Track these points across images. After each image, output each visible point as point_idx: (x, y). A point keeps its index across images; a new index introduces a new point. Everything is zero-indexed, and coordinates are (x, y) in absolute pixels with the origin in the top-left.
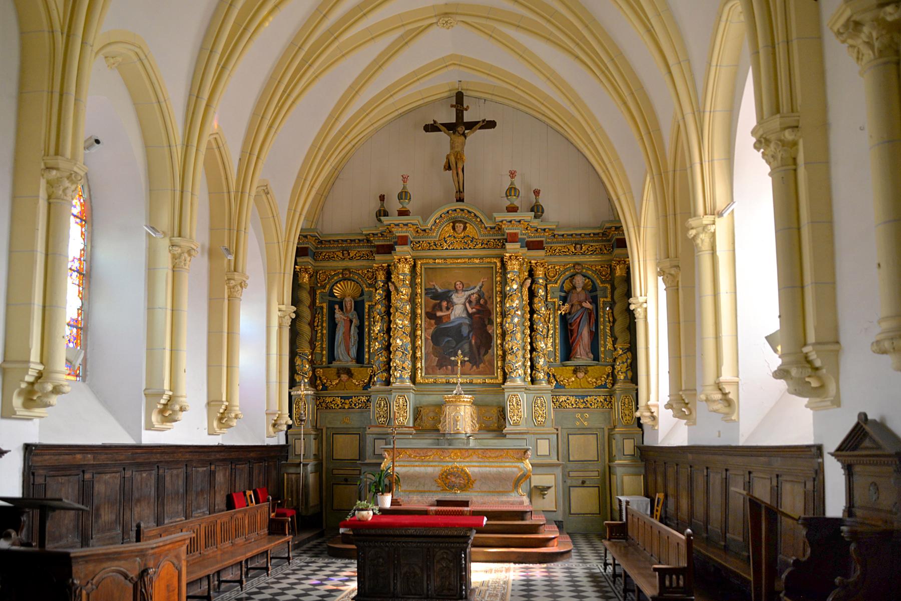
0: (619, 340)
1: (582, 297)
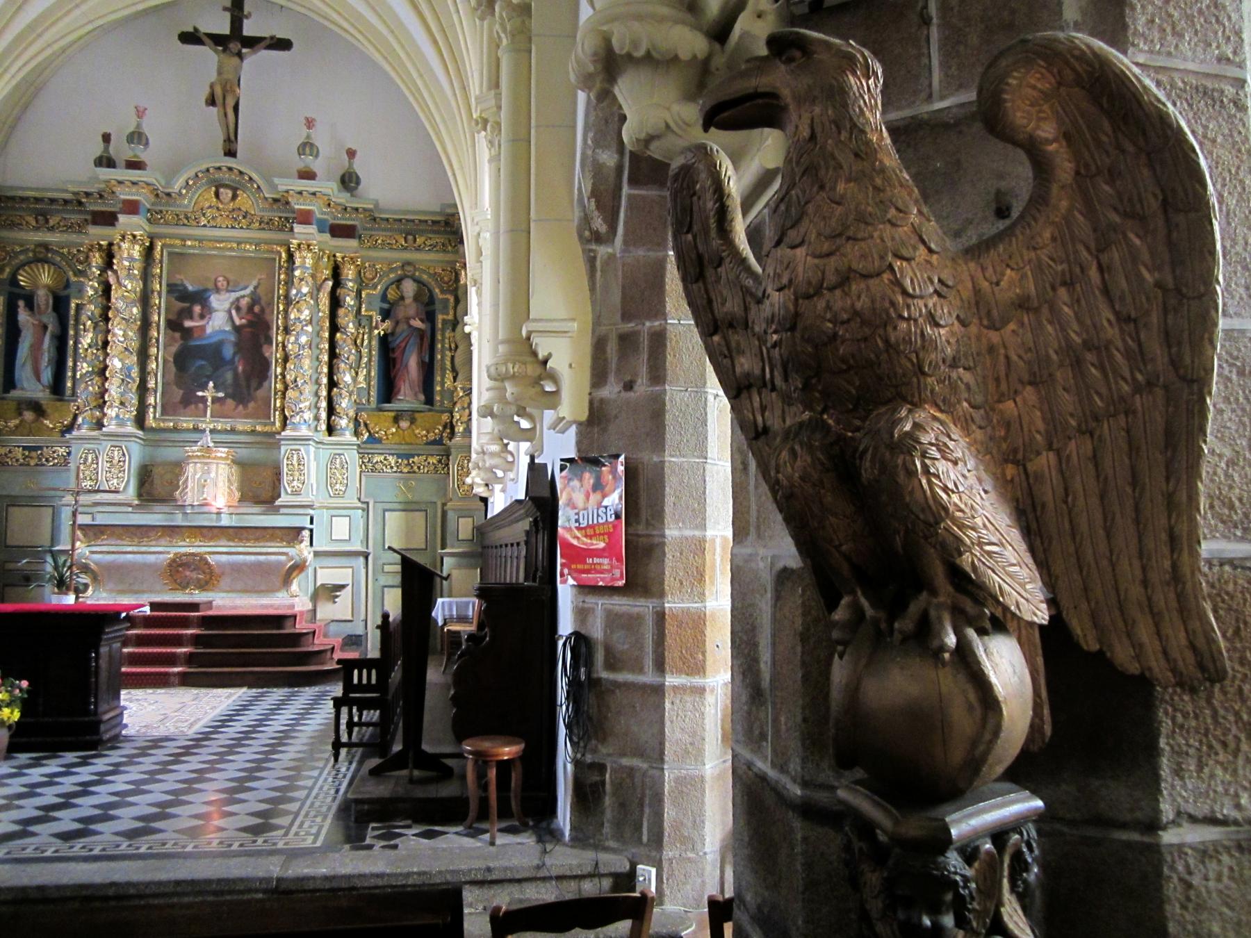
0: (460, 377)
1: (412, 311)
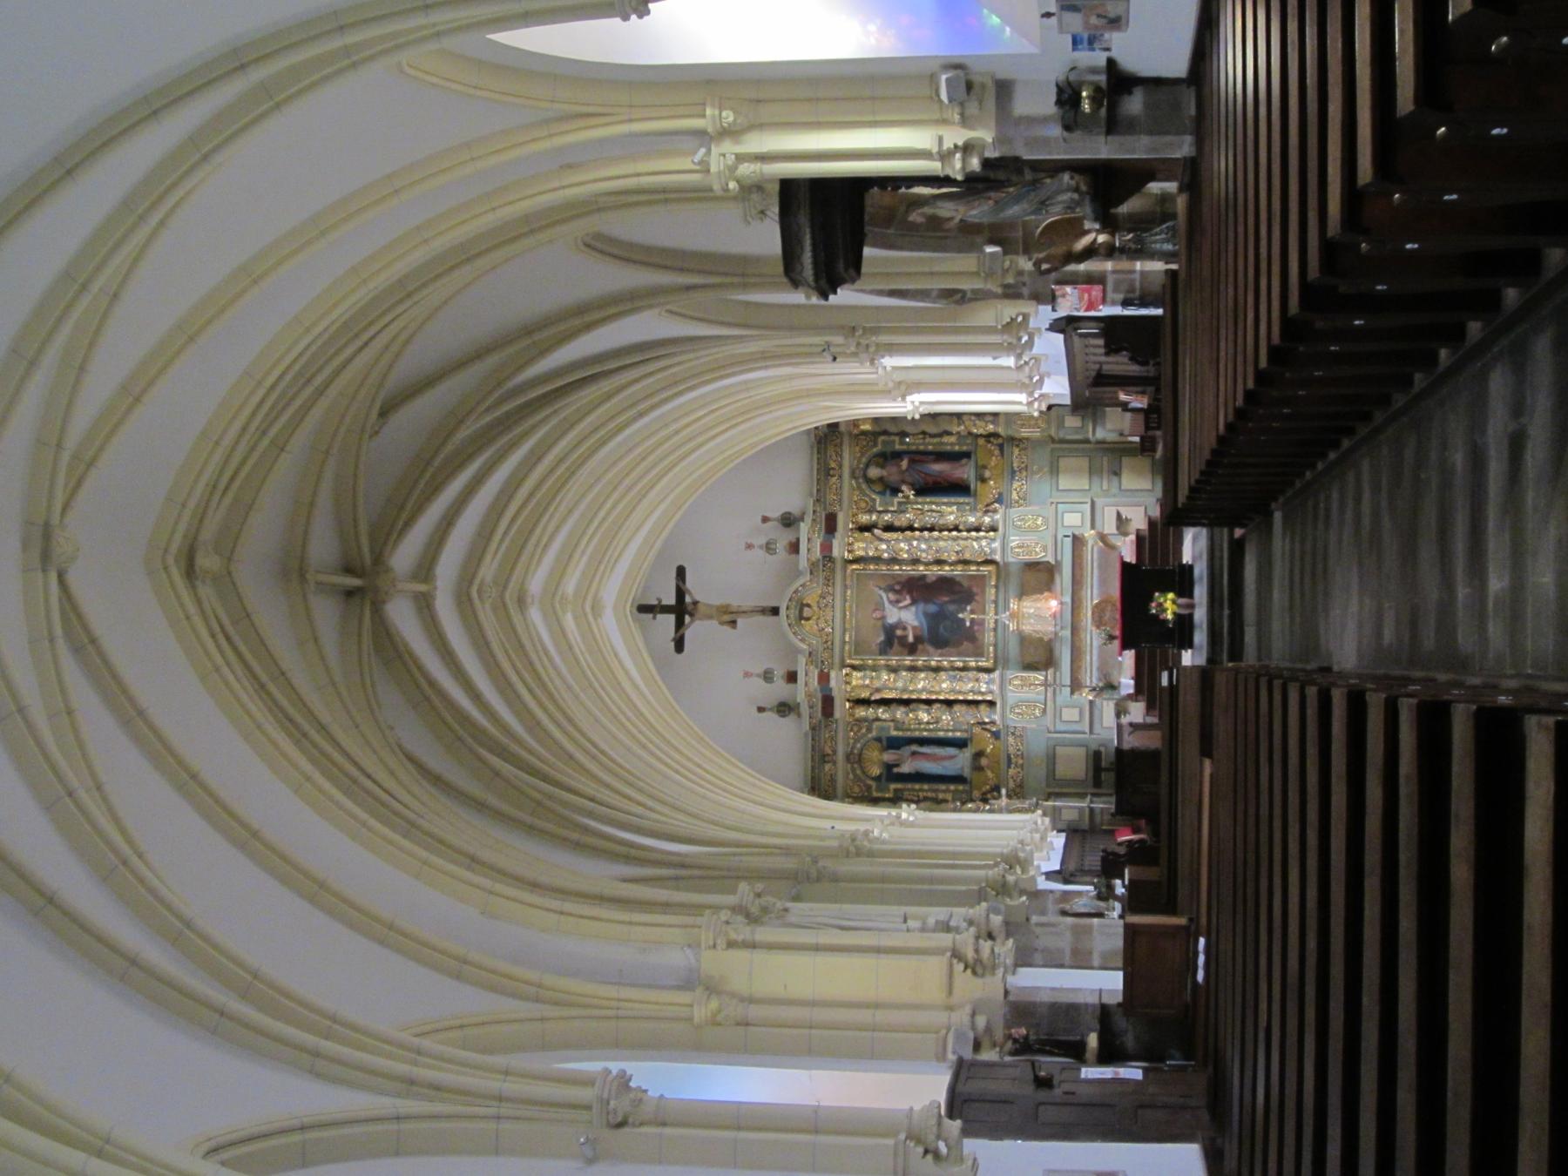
0: (948, 428)
1: (894, 469)
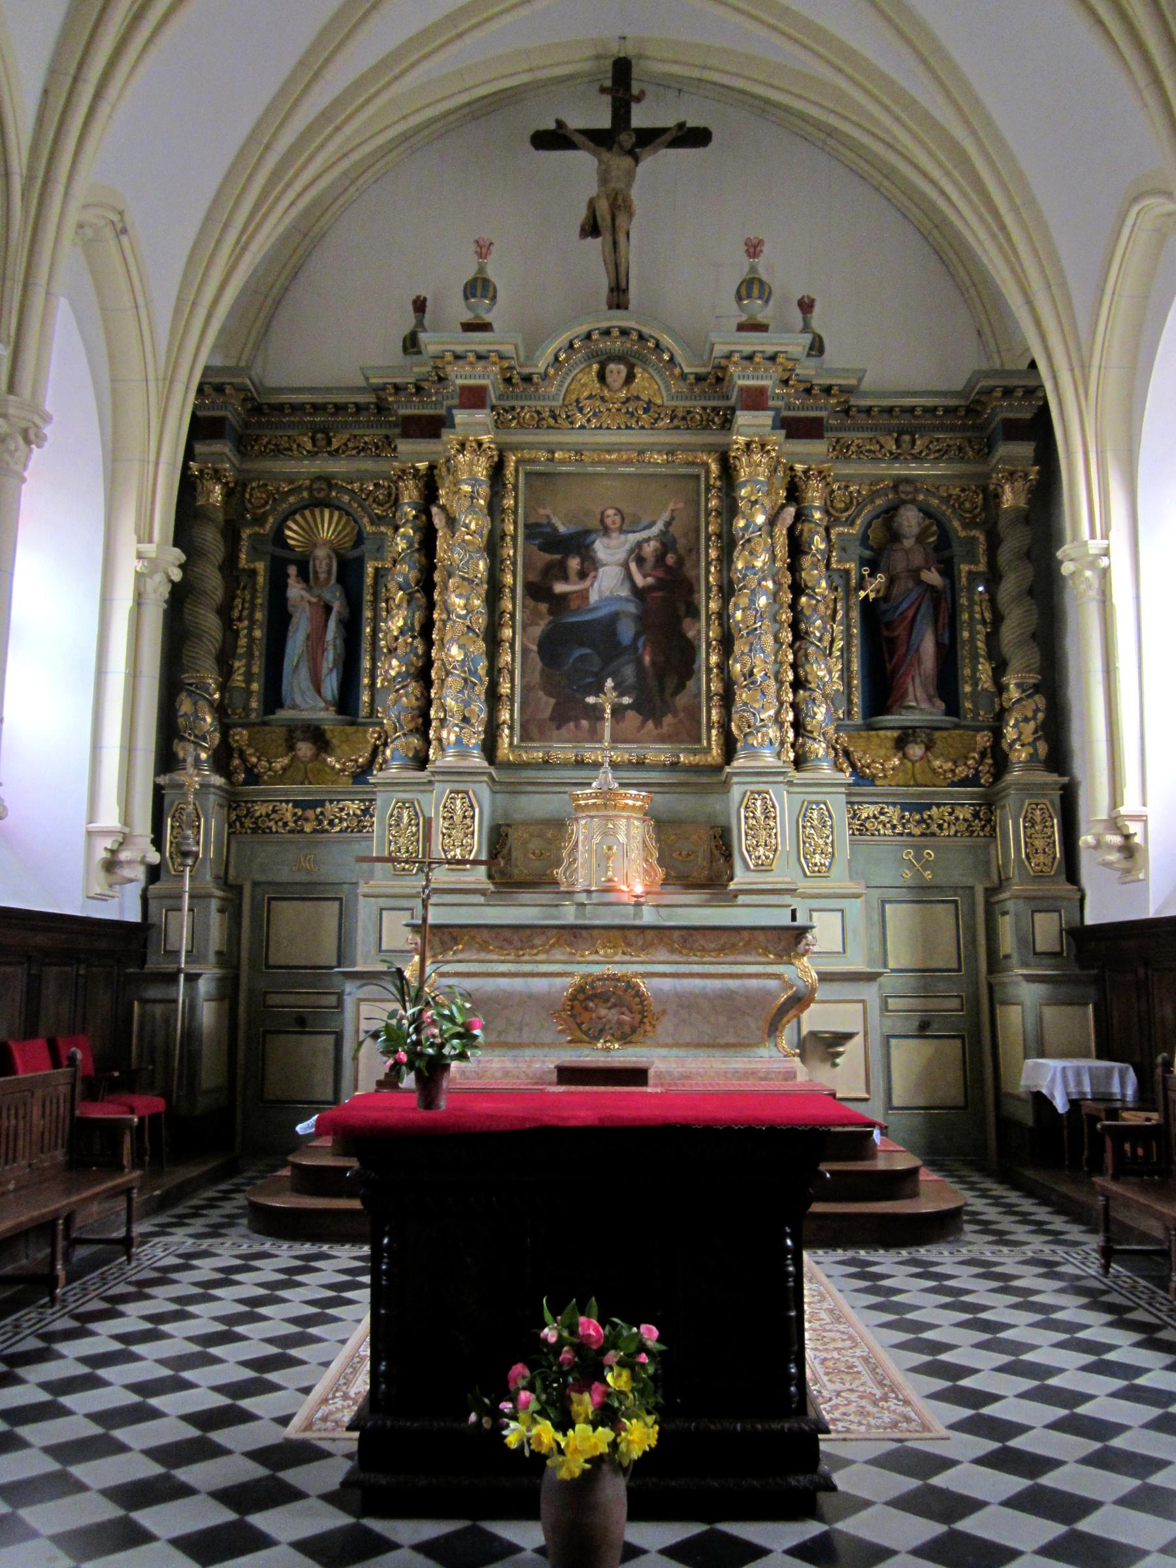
0: (1015, 663)
1: (918, 559)
